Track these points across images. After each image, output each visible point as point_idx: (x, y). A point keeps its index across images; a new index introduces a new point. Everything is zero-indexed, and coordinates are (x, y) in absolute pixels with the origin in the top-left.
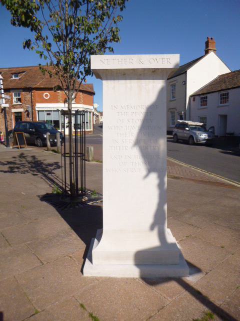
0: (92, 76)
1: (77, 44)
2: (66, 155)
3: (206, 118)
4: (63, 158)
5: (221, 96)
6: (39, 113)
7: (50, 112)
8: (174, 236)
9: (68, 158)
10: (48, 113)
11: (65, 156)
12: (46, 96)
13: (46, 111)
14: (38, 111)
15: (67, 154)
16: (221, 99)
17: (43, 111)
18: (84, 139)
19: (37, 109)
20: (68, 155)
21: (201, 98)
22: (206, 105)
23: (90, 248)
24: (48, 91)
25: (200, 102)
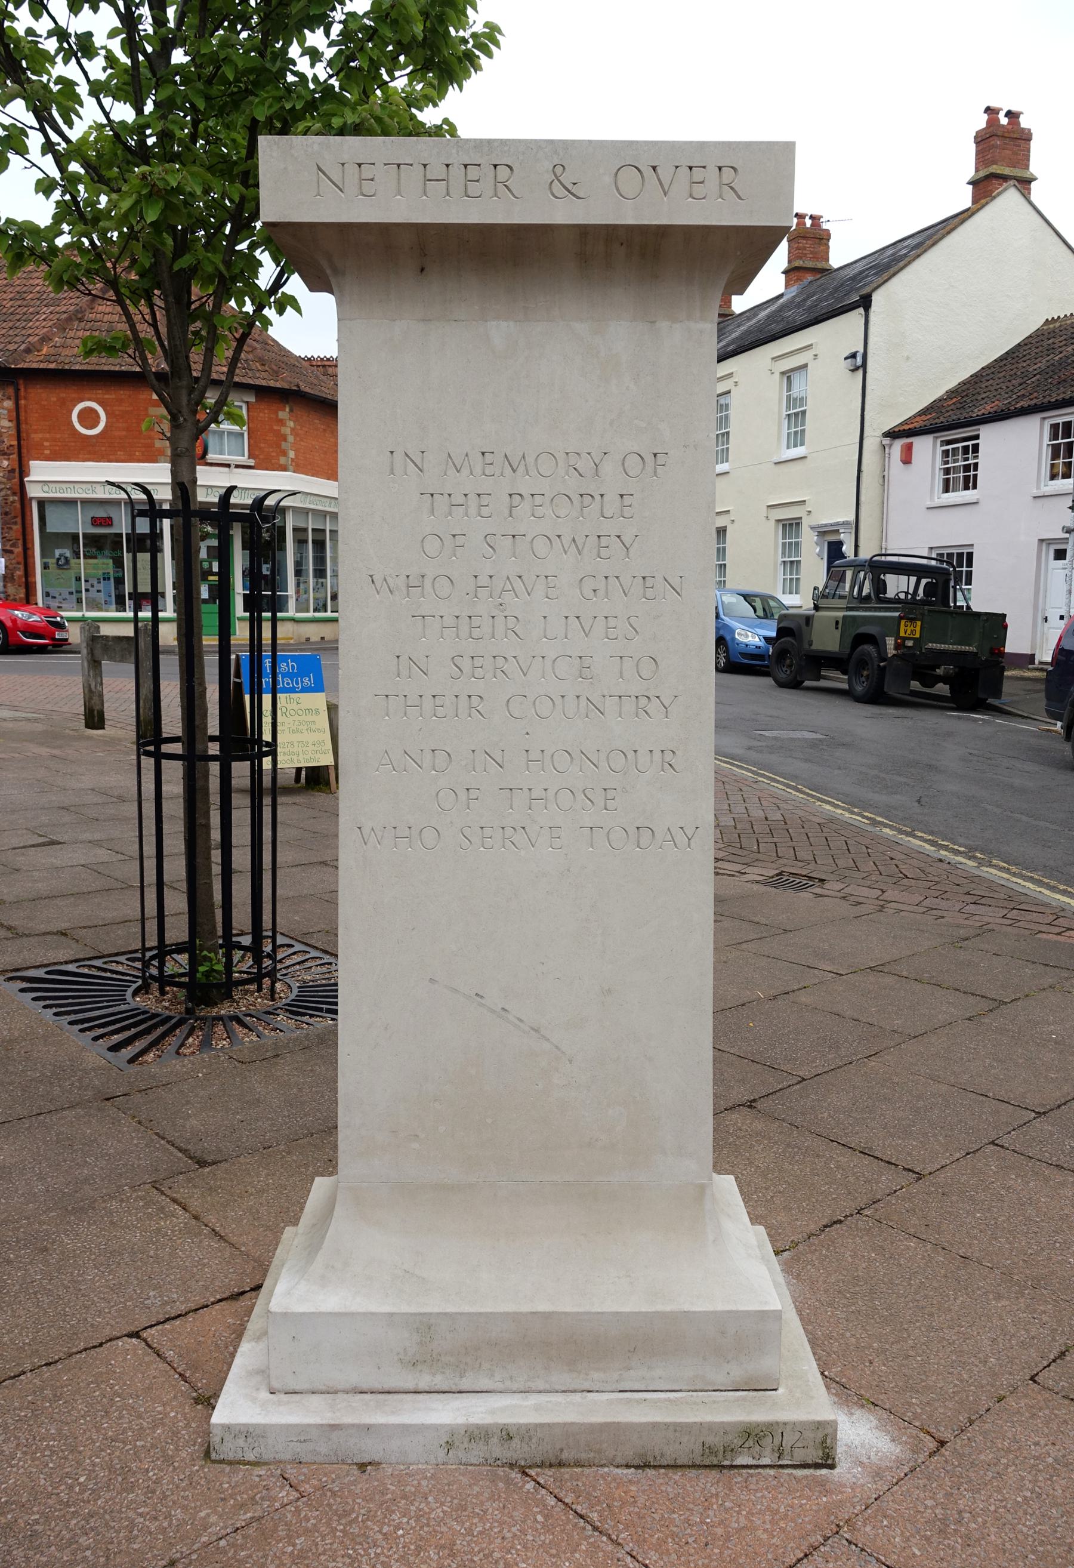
0: (489, 55)
1: (37, 1527)
2: (166, 748)
3: (970, 556)
4: (148, 763)
5: (1055, 437)
6: (49, 511)
7: (112, 512)
8: (755, 1219)
9: (178, 765)
10: (101, 513)
11: (159, 757)
12: (89, 418)
13: (86, 502)
14: (42, 503)
15: (150, 949)
16: (1055, 452)
17: (71, 503)
18: (267, 653)
19: (34, 492)
20: (177, 748)
21: (1055, 427)
22: (970, 483)
23: (195, 616)
24: (100, 393)
25: (1047, 453)
